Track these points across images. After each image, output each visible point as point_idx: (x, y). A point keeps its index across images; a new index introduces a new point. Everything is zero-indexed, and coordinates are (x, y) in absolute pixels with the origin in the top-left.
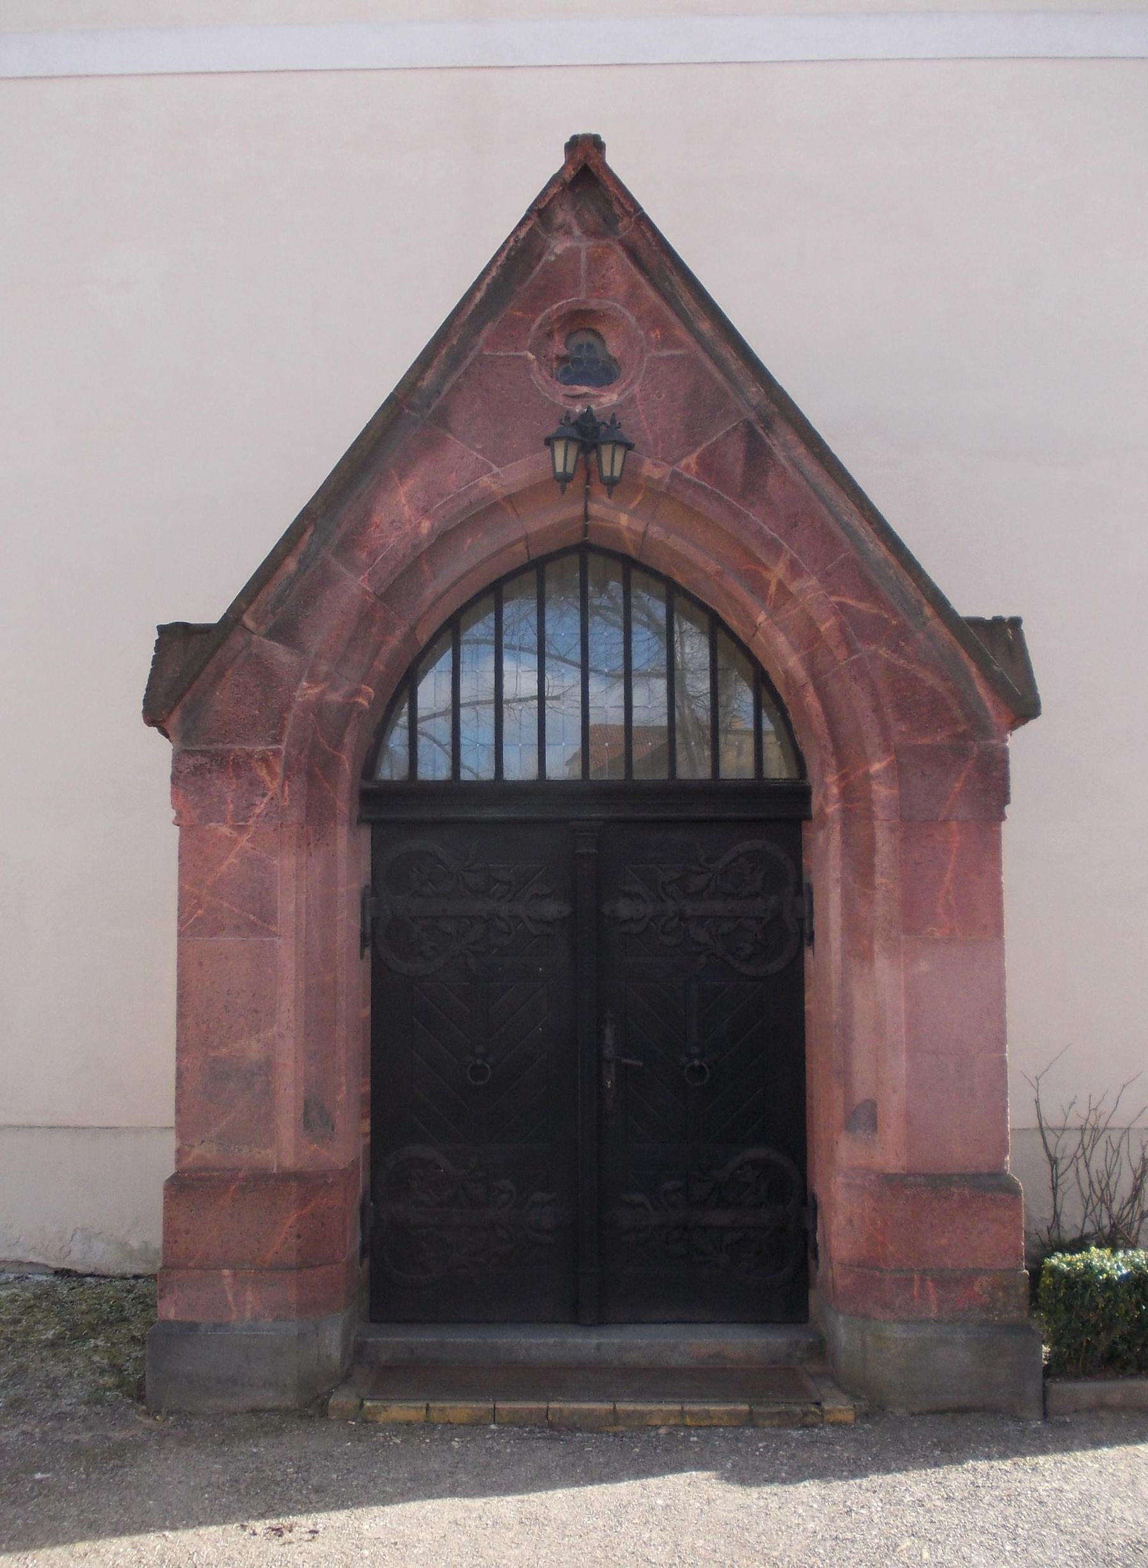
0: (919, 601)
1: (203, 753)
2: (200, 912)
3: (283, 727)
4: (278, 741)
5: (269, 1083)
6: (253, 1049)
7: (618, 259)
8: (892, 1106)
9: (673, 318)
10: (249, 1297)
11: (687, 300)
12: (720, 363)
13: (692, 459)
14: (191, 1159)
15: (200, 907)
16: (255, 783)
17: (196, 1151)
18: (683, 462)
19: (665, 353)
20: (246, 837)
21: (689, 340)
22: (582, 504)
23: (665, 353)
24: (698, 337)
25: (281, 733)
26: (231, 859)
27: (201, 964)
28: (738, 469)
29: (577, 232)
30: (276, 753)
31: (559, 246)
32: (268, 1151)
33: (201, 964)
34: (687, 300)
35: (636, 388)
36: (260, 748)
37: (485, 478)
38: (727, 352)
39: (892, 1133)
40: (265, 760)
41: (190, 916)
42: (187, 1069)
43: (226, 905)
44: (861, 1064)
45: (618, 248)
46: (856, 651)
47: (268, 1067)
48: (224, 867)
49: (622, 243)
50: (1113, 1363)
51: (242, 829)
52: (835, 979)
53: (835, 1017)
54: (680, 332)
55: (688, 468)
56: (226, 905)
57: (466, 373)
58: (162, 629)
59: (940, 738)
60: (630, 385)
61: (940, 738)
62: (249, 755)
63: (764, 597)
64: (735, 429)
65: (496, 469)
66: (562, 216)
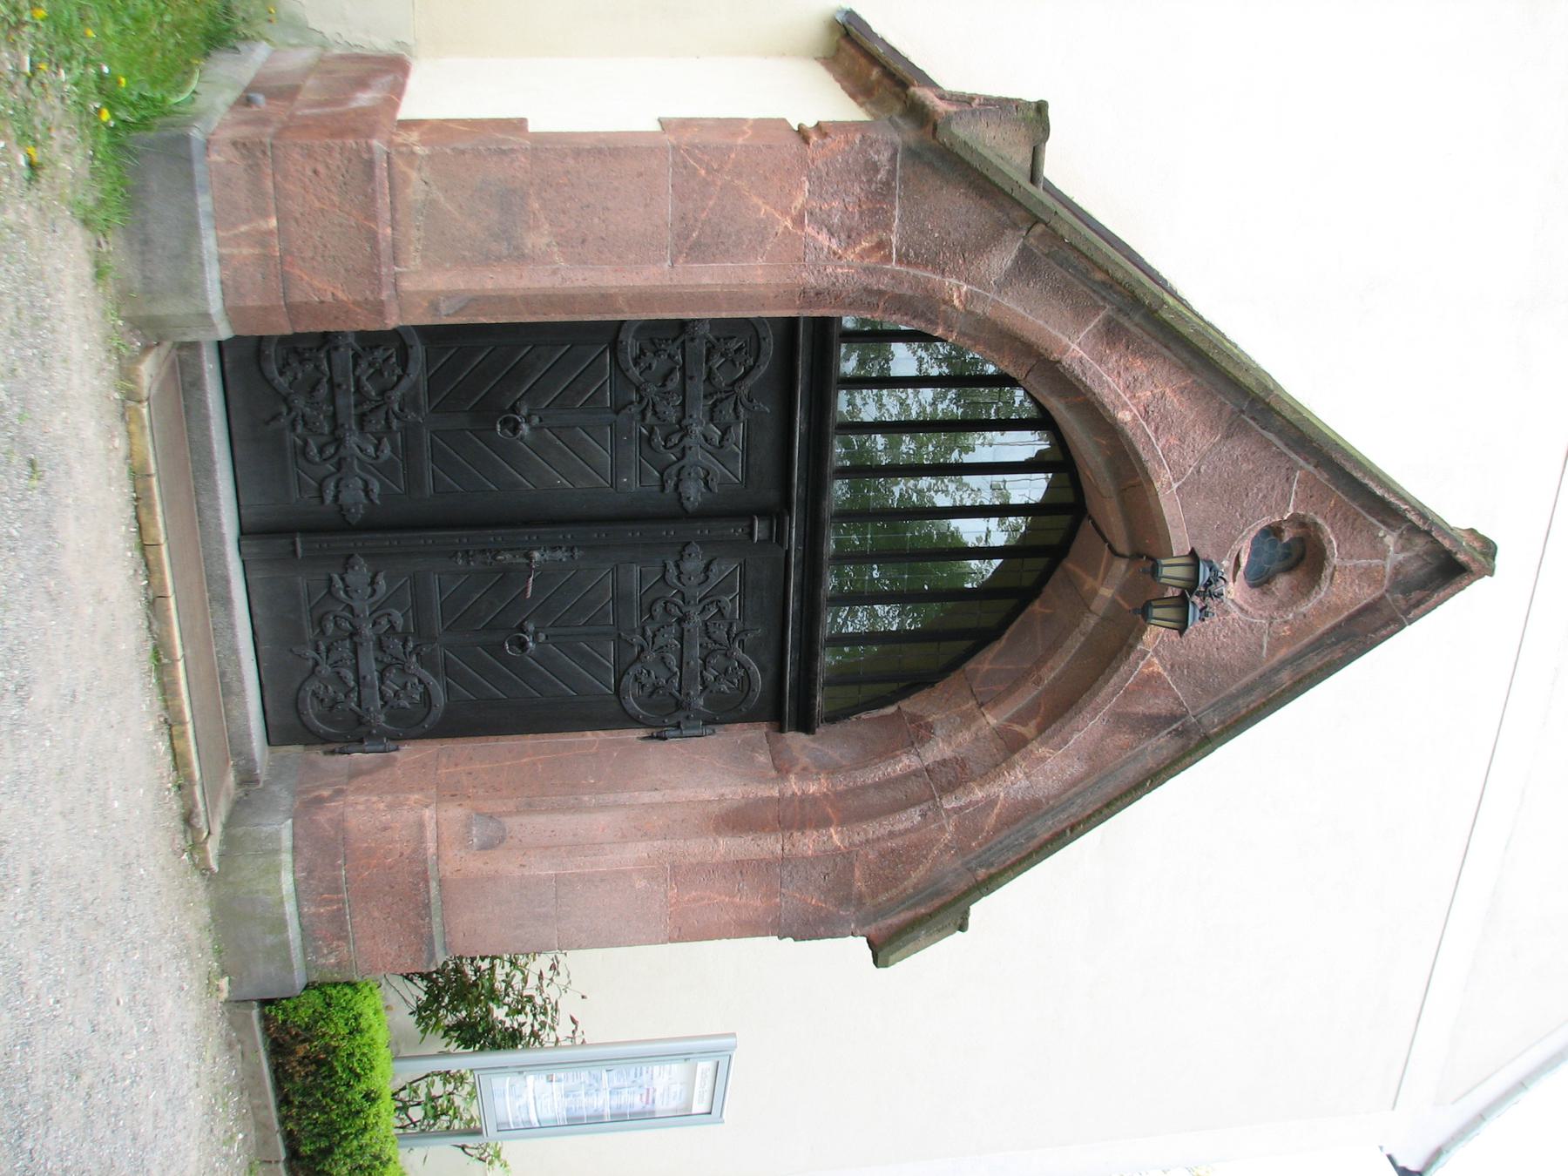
0: (992, 864)
1: (892, 173)
2: (703, 172)
3: (916, 265)
4: (899, 261)
5: (499, 259)
6: (538, 240)
7: (1367, 594)
8: (506, 864)
9: (1299, 646)
10: (246, 251)
11: (1315, 661)
12: (1248, 689)
13: (1158, 667)
14: (405, 169)
15: (708, 172)
16: (851, 236)
17: (414, 175)
18: (1155, 660)
19: (1265, 640)
20: (789, 224)
21: (1274, 661)
22: (1127, 553)
23: (1265, 640)
24: (1276, 670)
25: (909, 263)
26: (765, 208)
27: (640, 175)
28: (1140, 709)
29: (1401, 557)
30: (888, 258)
31: (1390, 540)
32: (418, 261)
33: (640, 175)
34: (1315, 661)
35: (1236, 613)
36: (894, 240)
37: (1169, 475)
38: (1255, 699)
39: (476, 864)
40: (881, 245)
41: (699, 161)
42: (512, 161)
43: (711, 203)
44: (540, 824)
45: (1378, 594)
46: (949, 817)
47: (520, 257)
48: (755, 200)
49: (1382, 597)
50: (279, 1049)
51: (799, 221)
52: (624, 797)
53: (586, 798)
54: (1283, 653)
55: (1150, 664)
56: (711, 203)
57: (1281, 454)
58: (1041, 108)
59: (859, 885)
60: (1241, 609)
61: (859, 885)
62: (887, 227)
63: (1011, 720)
64: (1181, 704)
65: (1175, 486)
66: (1420, 544)
